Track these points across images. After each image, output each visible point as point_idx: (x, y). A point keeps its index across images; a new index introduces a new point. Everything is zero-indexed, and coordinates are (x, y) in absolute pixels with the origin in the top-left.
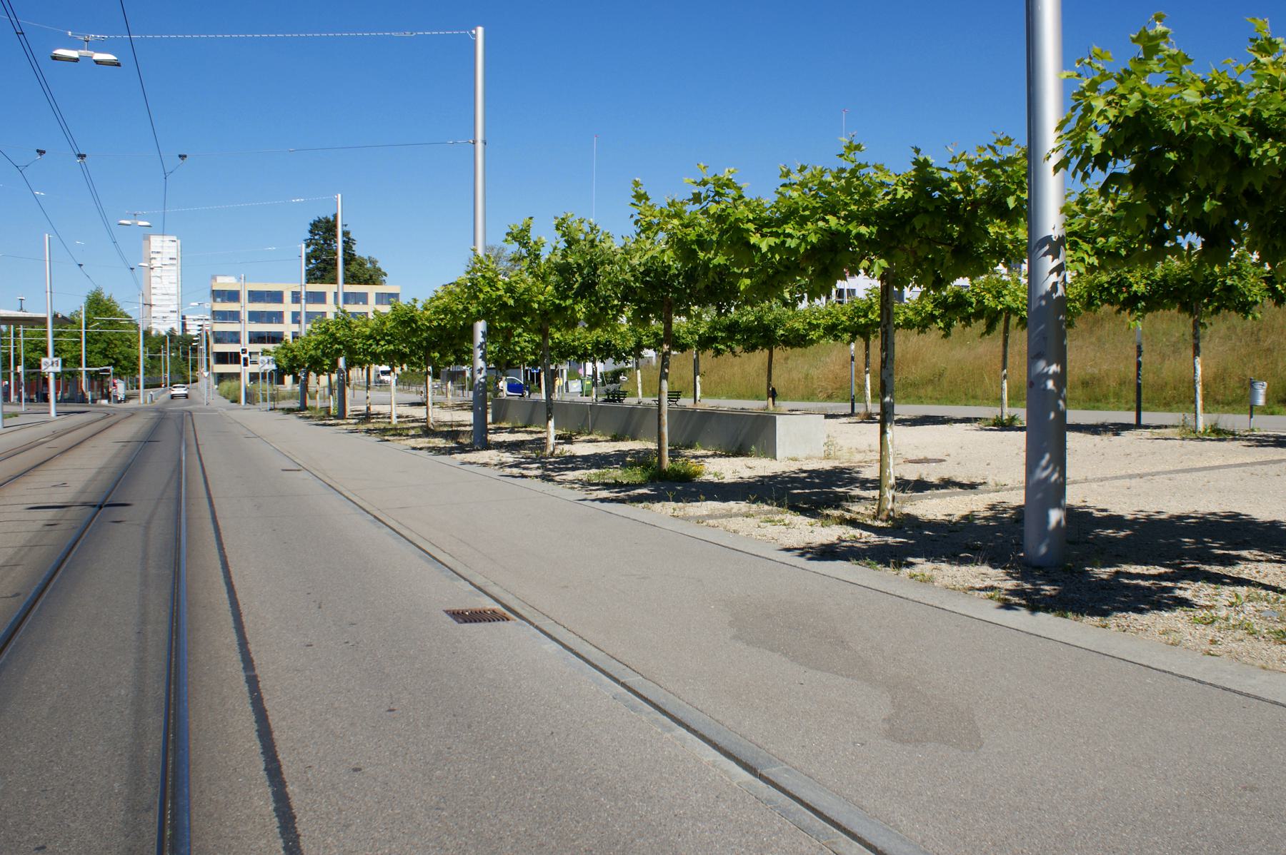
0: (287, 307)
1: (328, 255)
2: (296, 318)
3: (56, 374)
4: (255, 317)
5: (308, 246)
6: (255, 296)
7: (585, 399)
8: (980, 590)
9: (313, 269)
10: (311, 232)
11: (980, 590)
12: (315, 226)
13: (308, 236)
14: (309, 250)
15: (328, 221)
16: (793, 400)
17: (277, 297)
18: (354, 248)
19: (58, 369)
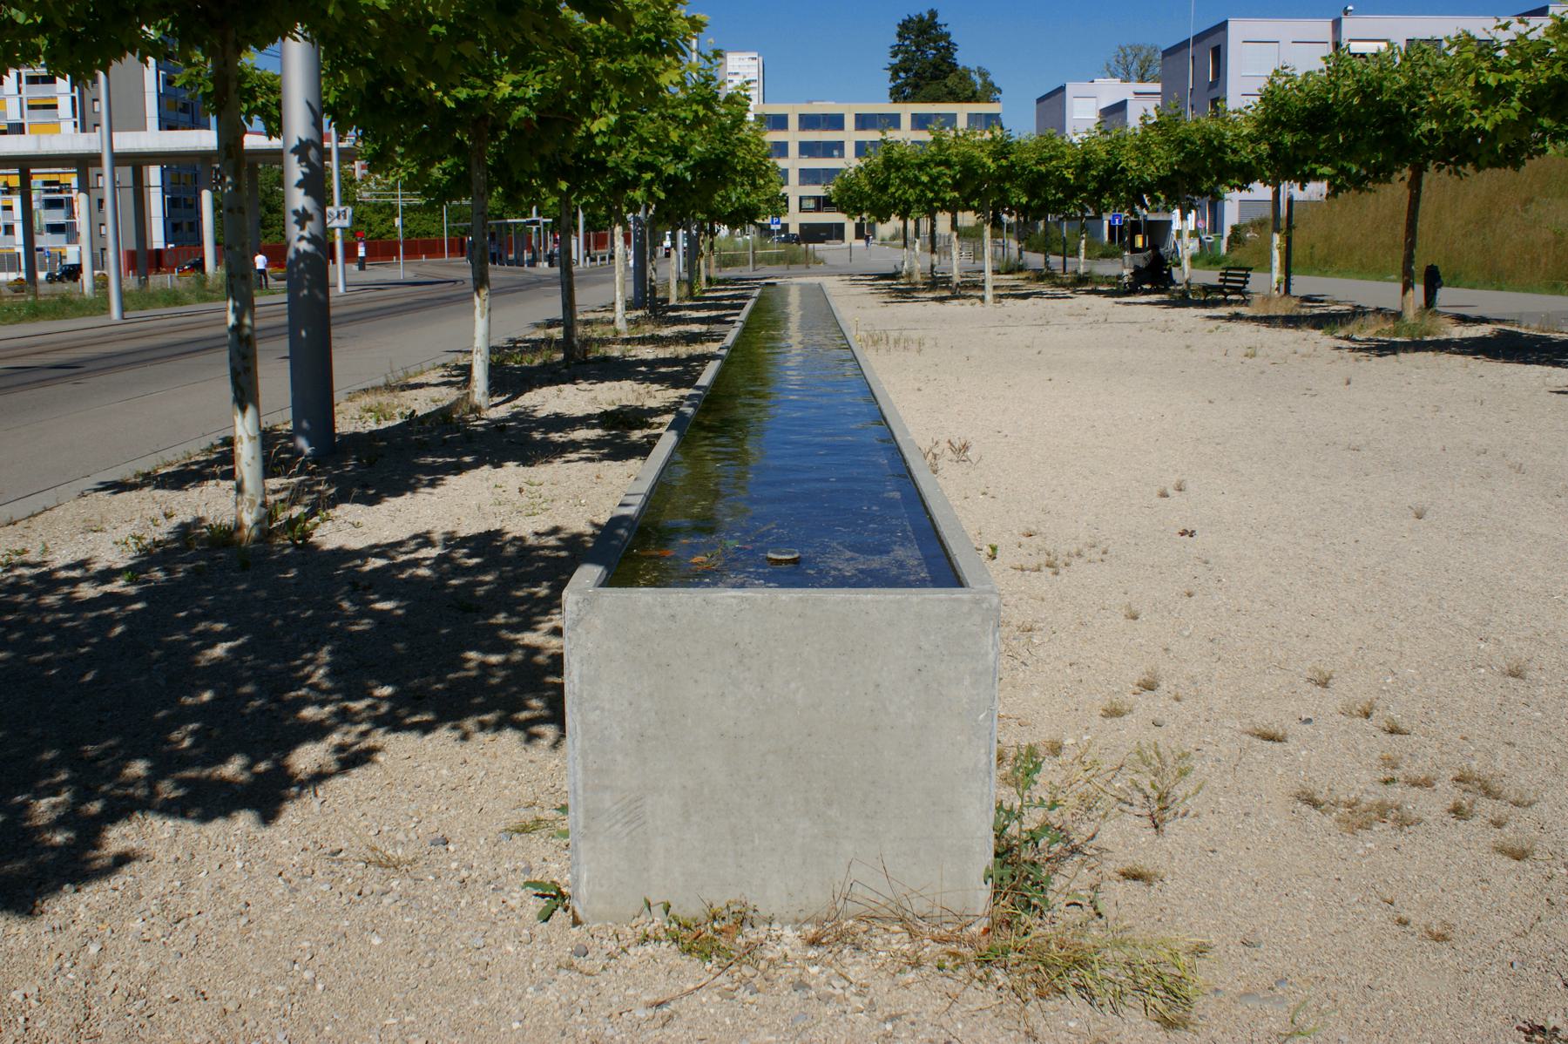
0: (850, 136)
1: (926, 65)
2: (861, 148)
3: (343, 229)
4: (807, 149)
5: (895, 55)
6: (808, 122)
7: (703, 279)
8: (428, 385)
9: (902, 85)
10: (900, 35)
11: (428, 385)
12: (905, 28)
13: (896, 41)
14: (896, 61)
15: (921, 20)
16: (1526, 288)
17: (836, 122)
18: (956, 55)
19: (346, 223)
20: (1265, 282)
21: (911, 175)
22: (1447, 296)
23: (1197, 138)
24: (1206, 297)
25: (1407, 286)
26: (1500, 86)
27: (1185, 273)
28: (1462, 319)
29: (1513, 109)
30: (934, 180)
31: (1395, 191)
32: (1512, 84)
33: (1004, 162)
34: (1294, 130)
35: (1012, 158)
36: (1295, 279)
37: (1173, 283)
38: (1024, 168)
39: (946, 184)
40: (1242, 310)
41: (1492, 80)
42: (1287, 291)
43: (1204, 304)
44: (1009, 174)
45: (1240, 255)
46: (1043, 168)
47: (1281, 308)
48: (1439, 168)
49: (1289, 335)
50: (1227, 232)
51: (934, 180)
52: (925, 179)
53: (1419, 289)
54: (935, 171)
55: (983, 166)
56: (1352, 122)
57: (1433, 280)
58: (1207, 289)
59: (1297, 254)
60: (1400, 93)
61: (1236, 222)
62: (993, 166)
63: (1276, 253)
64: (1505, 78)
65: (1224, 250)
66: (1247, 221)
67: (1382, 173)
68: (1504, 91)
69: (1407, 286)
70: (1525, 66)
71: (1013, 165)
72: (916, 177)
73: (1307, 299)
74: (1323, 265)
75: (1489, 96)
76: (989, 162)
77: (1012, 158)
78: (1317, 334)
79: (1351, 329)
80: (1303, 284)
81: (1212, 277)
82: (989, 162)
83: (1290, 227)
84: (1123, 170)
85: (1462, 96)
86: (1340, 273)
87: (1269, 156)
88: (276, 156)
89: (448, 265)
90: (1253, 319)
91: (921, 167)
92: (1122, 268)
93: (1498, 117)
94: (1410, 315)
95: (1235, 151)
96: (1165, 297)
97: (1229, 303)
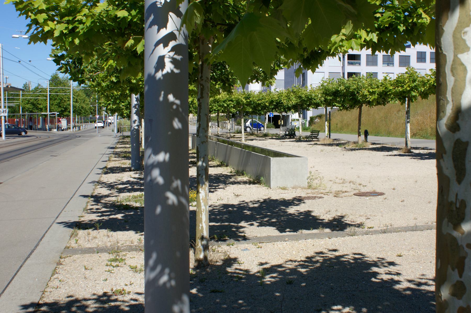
16: (396, 136)
20: (323, 136)
21: (221, 104)
22: (371, 138)
23: (303, 96)
24: (308, 139)
25: (359, 135)
26: (373, 91)
27: (300, 133)
28: (373, 144)
29: (376, 96)
30: (228, 105)
31: (356, 111)
32: (375, 91)
33: (248, 100)
34: (331, 96)
35: (251, 99)
36: (331, 134)
37: (295, 135)
38: (254, 102)
39: (232, 107)
40: (318, 143)
41: (371, 90)
42: (330, 137)
43: (306, 141)
44: (249, 104)
45: (313, 127)
46: (260, 102)
47: (328, 142)
48: (366, 105)
49: (330, 148)
50: (308, 119)
51: (228, 105)
52: (226, 105)
53: (363, 137)
54: (228, 103)
55: (242, 101)
56: (344, 95)
57: (366, 134)
58: (307, 137)
59: (332, 127)
60: (355, 89)
61: (311, 115)
62: (245, 102)
63: (326, 127)
64: (374, 90)
65: (307, 125)
66: (315, 115)
67: (352, 107)
68: (373, 93)
69: (359, 135)
70: (378, 87)
71: (251, 101)
72: (223, 105)
73: (336, 140)
74: (340, 130)
75: (372, 93)
76: (244, 100)
77: (251, 99)
78: (338, 147)
79: (346, 146)
80: (334, 136)
81: (308, 134)
82: (244, 100)
83: (330, 120)
84: (282, 103)
85: (366, 93)
86: (345, 133)
87: (324, 101)
88: (404, 134)
89: (48, 133)
90: (319, 144)
91: (224, 102)
92: (281, 132)
93: (373, 98)
94: (360, 142)
95: (315, 99)
96: (294, 140)
97: (314, 141)
